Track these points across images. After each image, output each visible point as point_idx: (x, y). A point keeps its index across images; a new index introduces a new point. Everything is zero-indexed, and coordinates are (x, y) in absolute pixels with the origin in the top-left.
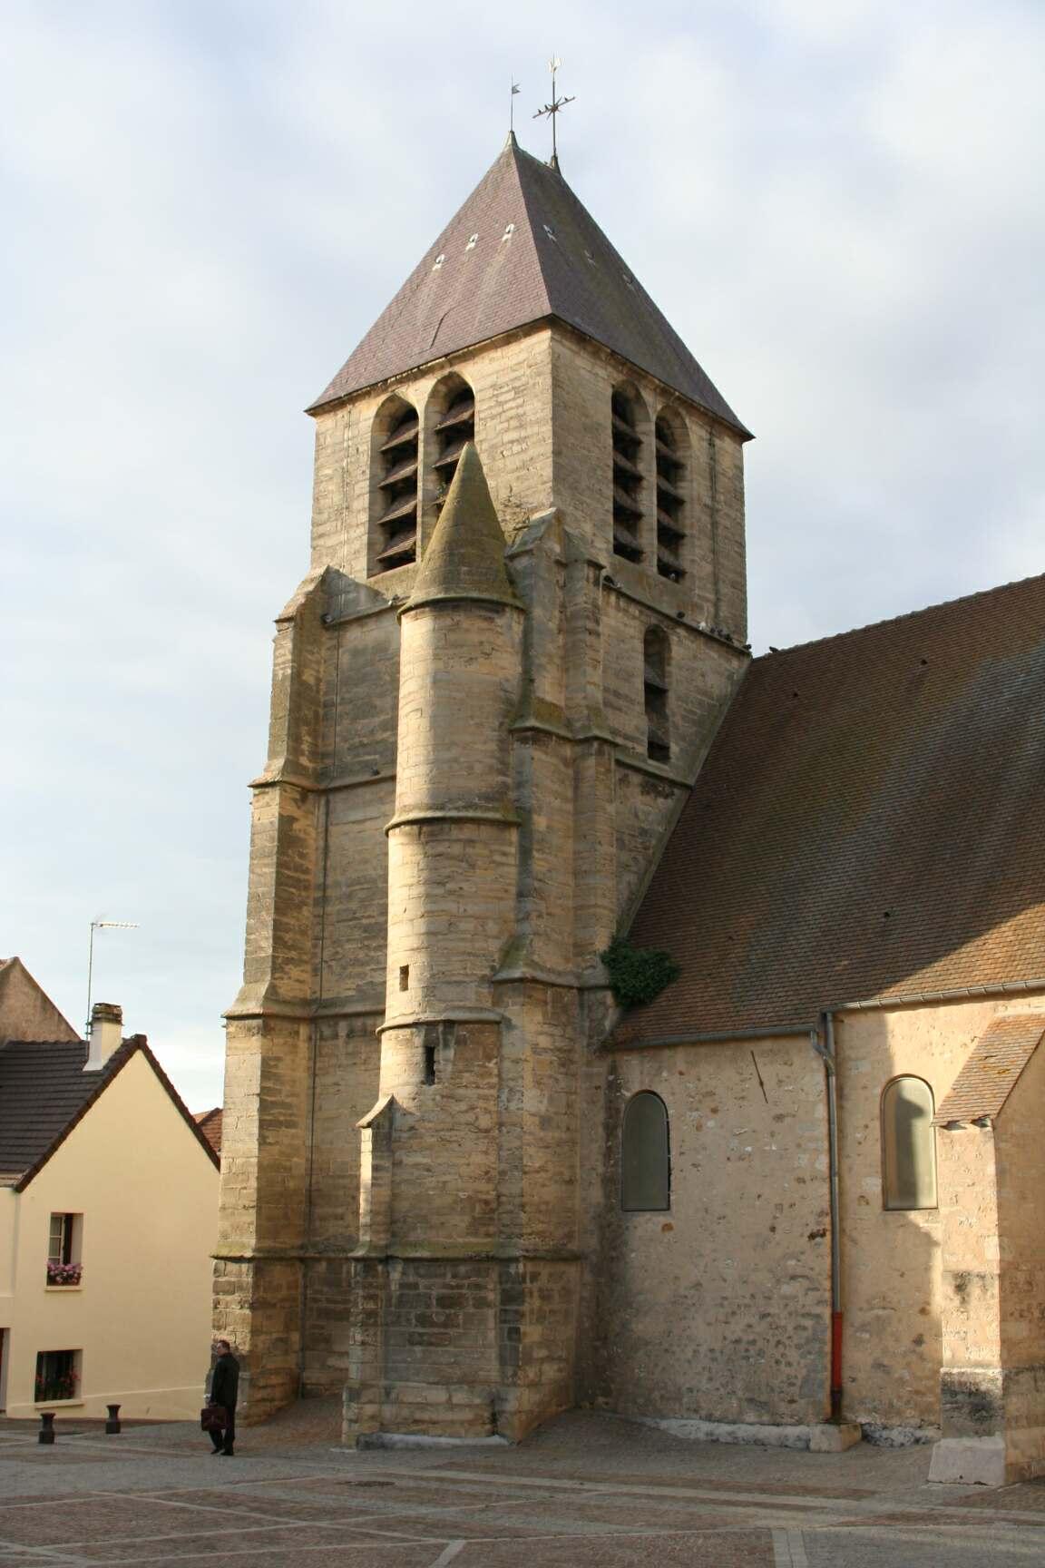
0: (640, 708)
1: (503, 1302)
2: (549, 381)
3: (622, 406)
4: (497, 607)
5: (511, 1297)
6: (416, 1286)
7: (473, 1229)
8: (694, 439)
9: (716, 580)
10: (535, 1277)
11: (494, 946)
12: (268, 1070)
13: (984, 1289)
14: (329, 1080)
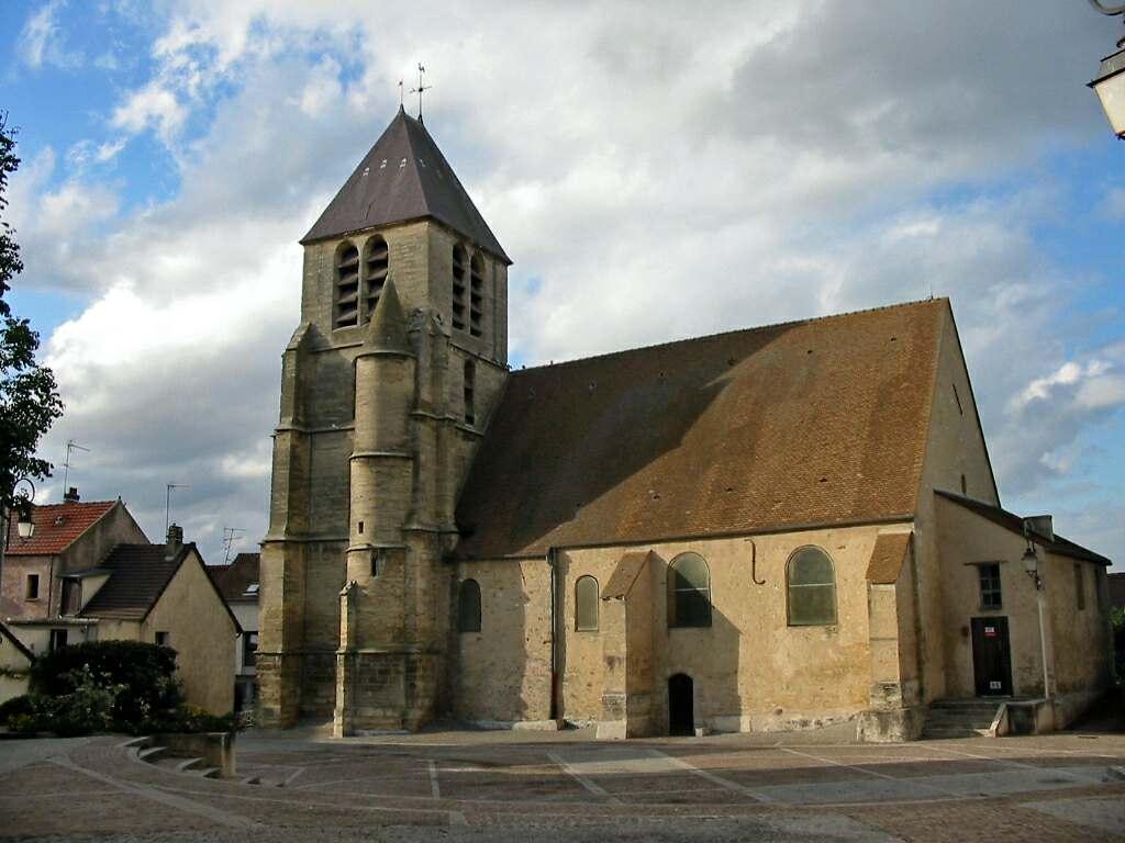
0: (463, 400)
1: (407, 671)
2: (427, 246)
3: (458, 253)
4: (404, 357)
5: (411, 669)
6: (368, 665)
7: (395, 639)
8: (486, 266)
9: (494, 336)
10: (420, 661)
11: (402, 514)
12: (287, 567)
13: (620, 663)
14: (314, 571)
